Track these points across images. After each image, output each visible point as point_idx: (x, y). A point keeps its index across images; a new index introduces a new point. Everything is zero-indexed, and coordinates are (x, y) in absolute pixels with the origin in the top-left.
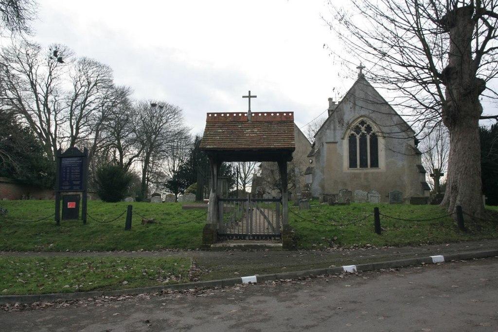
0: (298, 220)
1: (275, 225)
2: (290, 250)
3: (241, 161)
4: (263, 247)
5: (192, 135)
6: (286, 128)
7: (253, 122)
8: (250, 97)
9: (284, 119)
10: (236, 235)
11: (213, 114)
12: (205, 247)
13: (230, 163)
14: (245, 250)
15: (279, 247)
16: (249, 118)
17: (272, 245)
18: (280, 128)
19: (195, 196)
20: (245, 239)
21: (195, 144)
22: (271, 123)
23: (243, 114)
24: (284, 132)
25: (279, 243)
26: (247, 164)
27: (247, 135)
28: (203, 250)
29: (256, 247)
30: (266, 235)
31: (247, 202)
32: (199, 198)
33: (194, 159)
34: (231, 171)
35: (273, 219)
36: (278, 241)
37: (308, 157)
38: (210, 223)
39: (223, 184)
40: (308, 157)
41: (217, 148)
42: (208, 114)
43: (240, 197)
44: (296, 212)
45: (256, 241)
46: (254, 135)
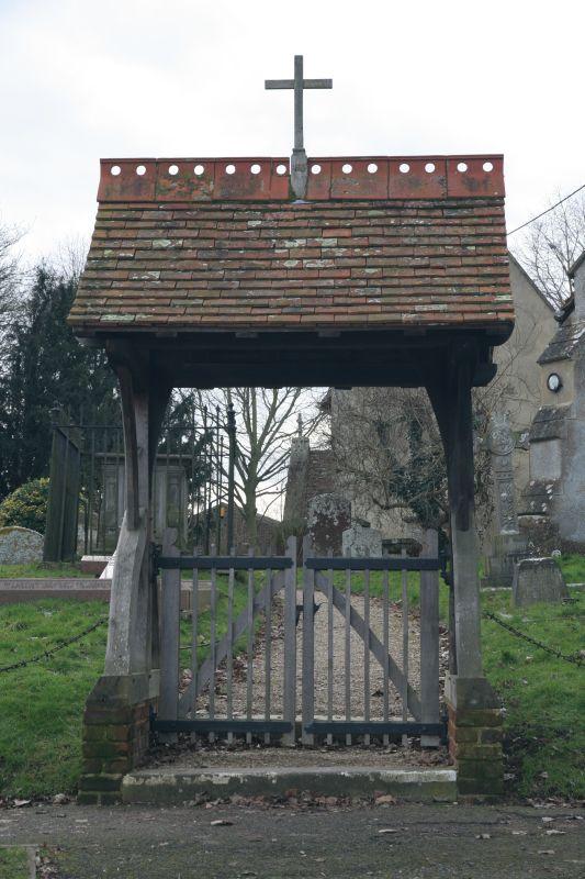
0: (516, 652)
1: (415, 678)
2: (491, 802)
3: (237, 385)
4: (368, 787)
5: (19, 265)
6: (468, 230)
7: (315, 205)
8: (299, 84)
9: (457, 189)
10: (240, 729)
11: (128, 164)
12: (95, 790)
13: (187, 391)
14: (283, 801)
15: (441, 785)
16: (298, 185)
17: (411, 775)
18: (440, 231)
19: (37, 538)
20: (278, 745)
21: (34, 304)
22: (395, 206)
23: (269, 163)
24: (457, 251)
25: (437, 763)
26: (263, 396)
27: (287, 264)
28: (87, 801)
29: (333, 785)
30: (257, 724)
31: (291, 573)
32: (61, 550)
33: (32, 370)
34: (193, 427)
35: (403, 640)
36: (435, 754)
37: (542, 362)
38: (122, 673)
39: (169, 485)
40: (542, 362)
41: (154, 324)
42: (106, 164)
43: (228, 544)
44: (506, 617)
45: (328, 756)
46: (319, 264)
